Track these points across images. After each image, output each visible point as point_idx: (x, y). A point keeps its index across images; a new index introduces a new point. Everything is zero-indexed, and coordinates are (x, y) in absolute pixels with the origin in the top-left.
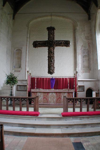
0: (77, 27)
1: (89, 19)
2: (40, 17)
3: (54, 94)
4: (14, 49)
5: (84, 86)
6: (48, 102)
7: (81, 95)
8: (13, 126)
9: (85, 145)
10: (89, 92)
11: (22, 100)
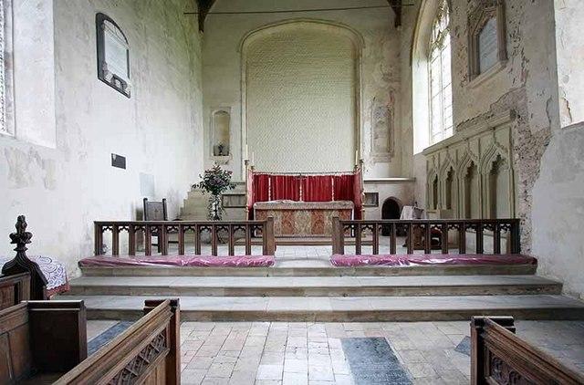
0: (364, 50)
1: (398, 23)
2: (268, 25)
3: (309, 214)
4: (212, 111)
5: (377, 194)
6: (292, 232)
7: (372, 213)
8: (211, 295)
9: (396, 347)
10: (392, 208)
11: (235, 227)
